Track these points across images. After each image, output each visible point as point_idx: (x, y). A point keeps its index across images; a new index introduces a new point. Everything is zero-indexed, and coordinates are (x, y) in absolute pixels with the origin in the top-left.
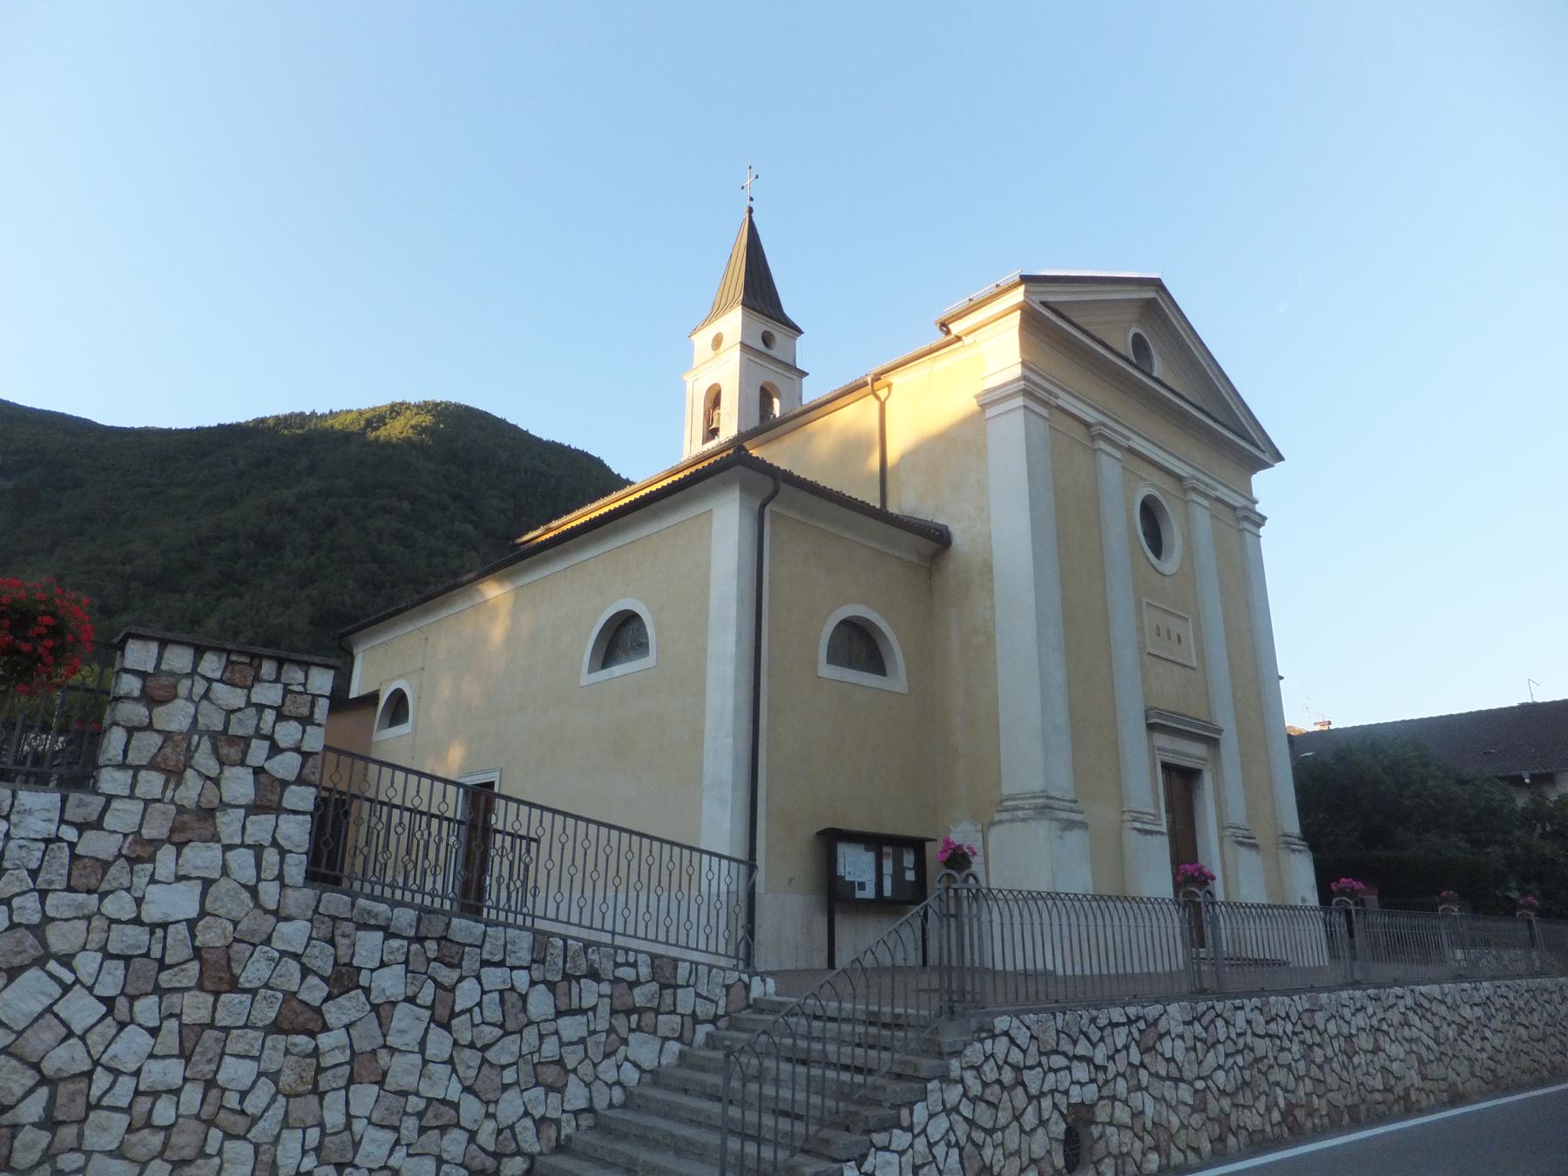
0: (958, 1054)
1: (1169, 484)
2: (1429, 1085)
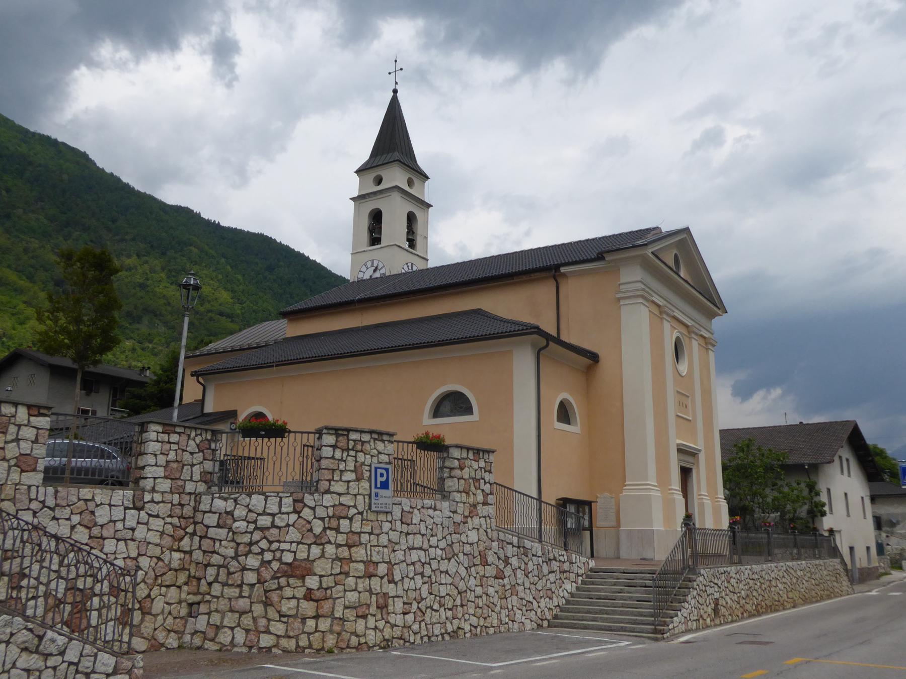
1: (684, 331)
2: (789, 600)
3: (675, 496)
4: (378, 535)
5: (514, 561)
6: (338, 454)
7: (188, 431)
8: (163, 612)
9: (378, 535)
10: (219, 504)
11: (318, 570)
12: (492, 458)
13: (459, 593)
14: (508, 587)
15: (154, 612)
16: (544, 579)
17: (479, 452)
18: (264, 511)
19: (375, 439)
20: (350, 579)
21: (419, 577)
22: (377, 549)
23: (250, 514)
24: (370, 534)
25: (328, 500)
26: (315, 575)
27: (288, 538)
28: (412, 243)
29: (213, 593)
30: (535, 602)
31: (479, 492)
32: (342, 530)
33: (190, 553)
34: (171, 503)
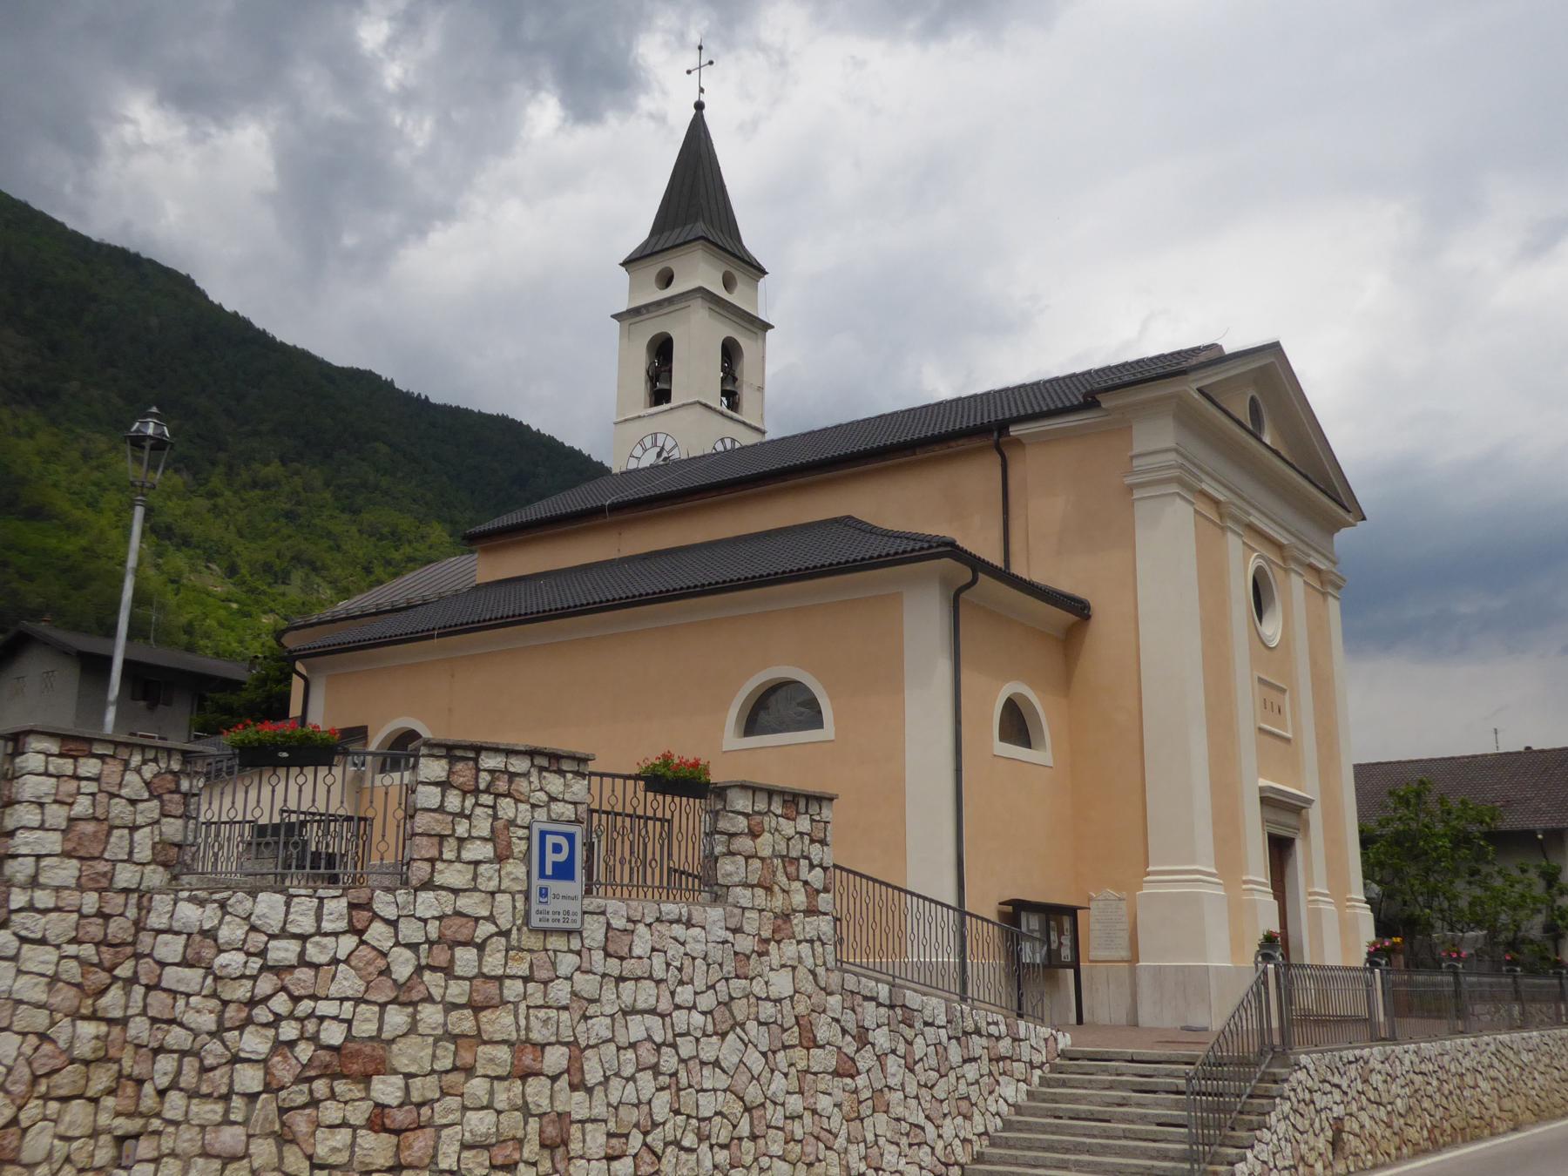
0: (1286, 1080)
2: (1503, 1115)
3: (1257, 897)
4: (545, 983)
5: (881, 1038)
6: (453, 801)
7: (123, 753)
8: (49, 1157)
9: (545, 983)
10: (189, 914)
11: (403, 1063)
12: (827, 813)
13: (747, 1109)
14: (866, 1094)
15: (26, 1157)
16: (952, 1075)
17: (795, 801)
18: (283, 929)
19: (542, 769)
20: (476, 1081)
21: (648, 1075)
22: (542, 1013)
23: (252, 935)
24: (526, 980)
25: (427, 904)
26: (395, 1072)
27: (334, 990)
28: (732, 397)
29: (168, 1115)
30: (929, 1127)
31: (797, 885)
32: (458, 971)
33: (124, 1022)
34: (79, 911)
